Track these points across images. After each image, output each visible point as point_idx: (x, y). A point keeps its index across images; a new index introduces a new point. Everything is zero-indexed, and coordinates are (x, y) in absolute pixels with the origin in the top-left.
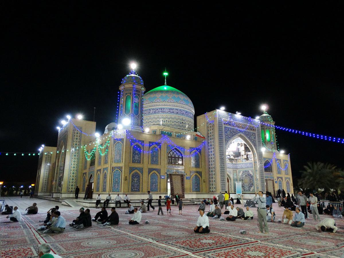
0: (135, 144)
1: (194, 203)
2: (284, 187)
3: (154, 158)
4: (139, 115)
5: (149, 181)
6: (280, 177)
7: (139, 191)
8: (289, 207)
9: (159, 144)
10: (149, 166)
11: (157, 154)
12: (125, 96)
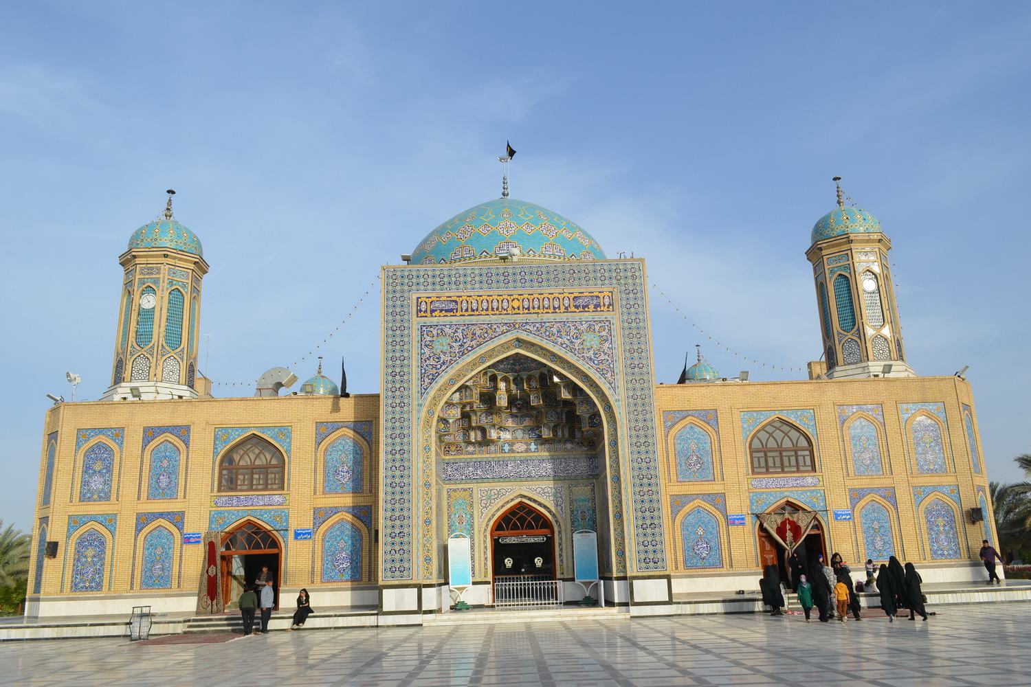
0: (93, 442)
2: (908, 529)
3: (161, 477)
4: (182, 351)
5: (139, 553)
7: (99, 586)
9: (183, 432)
11: (174, 466)
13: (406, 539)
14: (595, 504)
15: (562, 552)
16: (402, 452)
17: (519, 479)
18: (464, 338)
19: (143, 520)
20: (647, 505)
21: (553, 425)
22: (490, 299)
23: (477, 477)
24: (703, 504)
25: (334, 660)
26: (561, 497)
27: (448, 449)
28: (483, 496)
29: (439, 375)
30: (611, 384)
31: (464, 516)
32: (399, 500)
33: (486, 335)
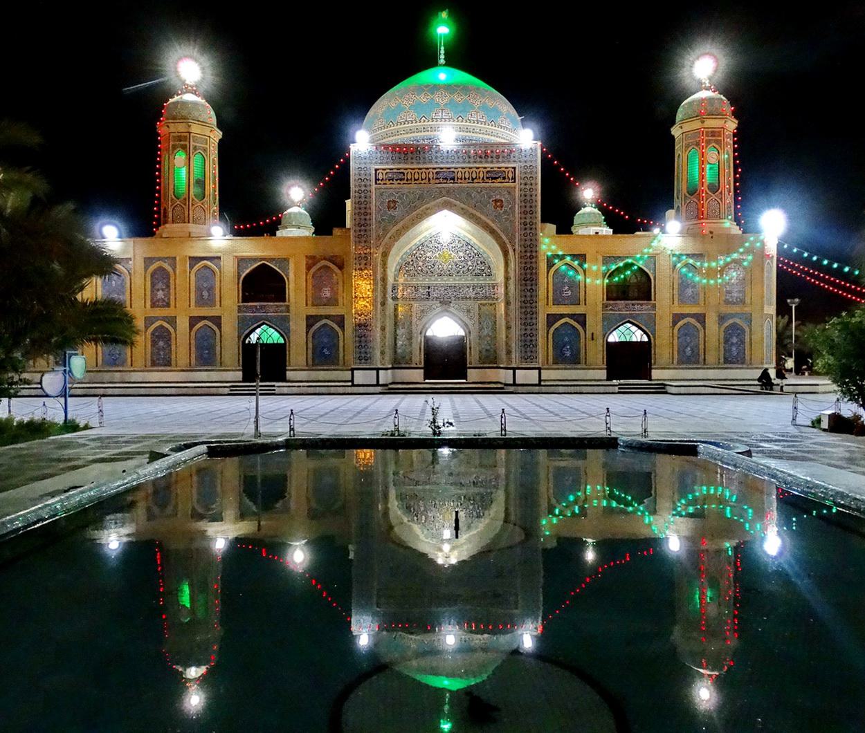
1: (274, 390)
12: (686, 151)
19: (677, 318)
22: (463, 171)
24: (210, 324)
25: (331, 413)
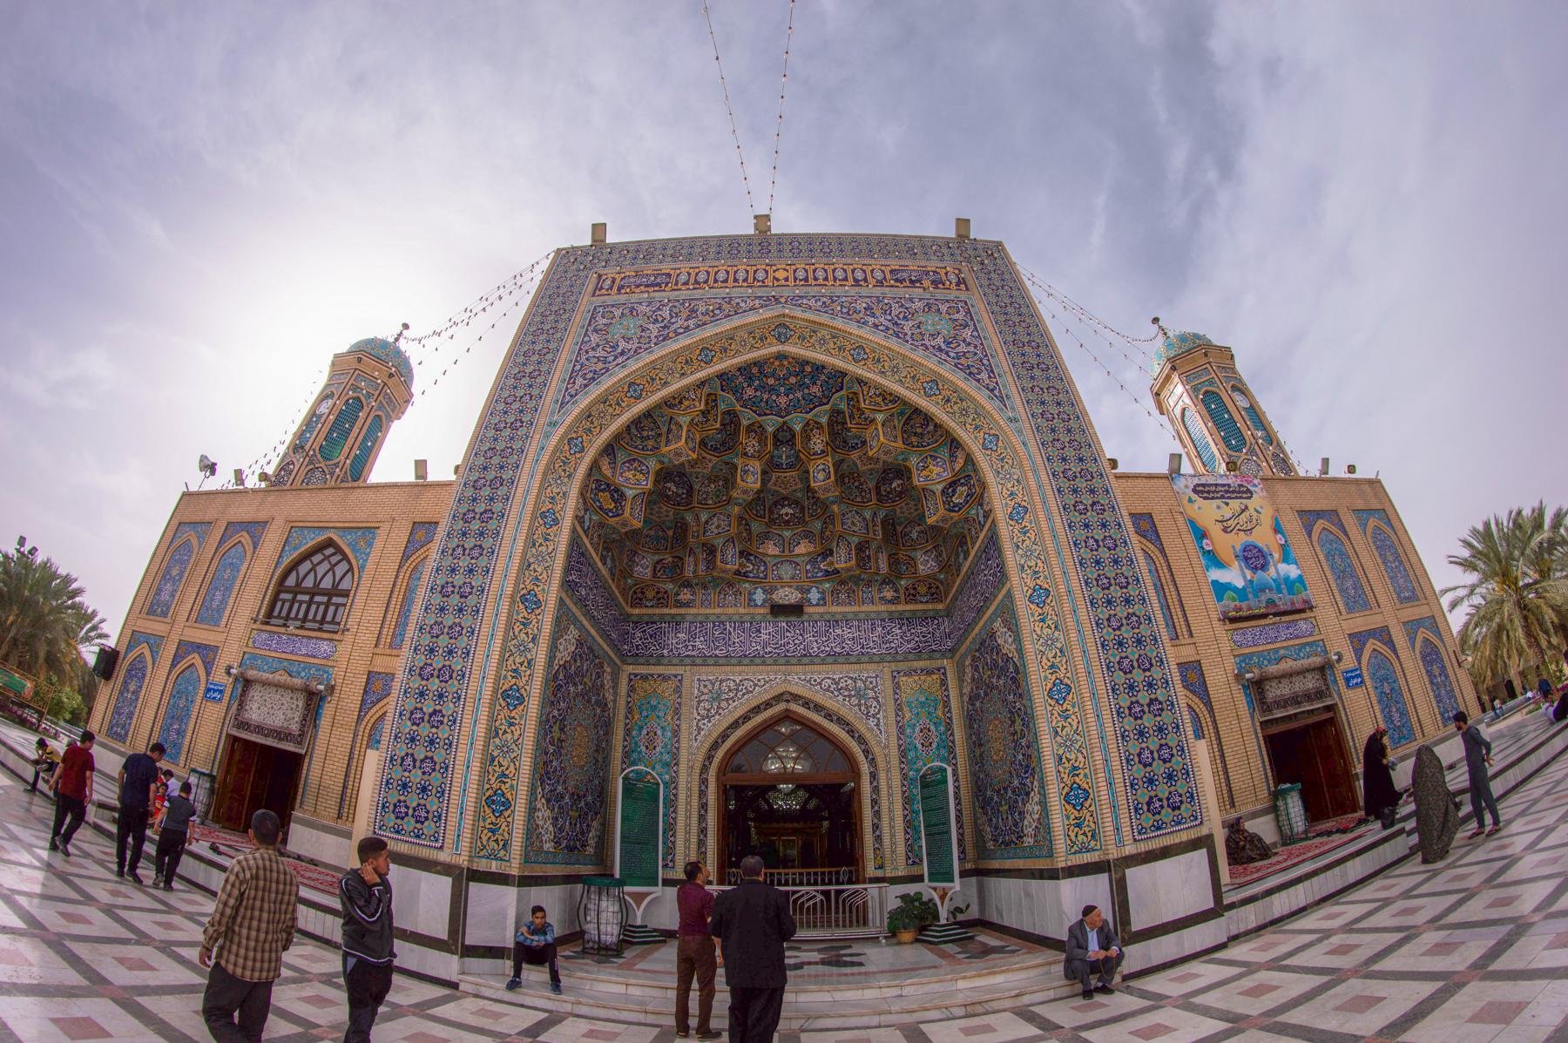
6: (1372, 633)
8: (65, 769)
10: (140, 622)
13: (443, 733)
14: (950, 711)
15: (879, 819)
16: (487, 516)
17: (782, 661)
18: (672, 317)
20: (1133, 653)
21: (856, 540)
23: (694, 653)
26: (876, 699)
27: (640, 595)
28: (703, 694)
29: (607, 371)
30: (992, 391)
31: (659, 733)
32: (451, 628)
33: (717, 312)
